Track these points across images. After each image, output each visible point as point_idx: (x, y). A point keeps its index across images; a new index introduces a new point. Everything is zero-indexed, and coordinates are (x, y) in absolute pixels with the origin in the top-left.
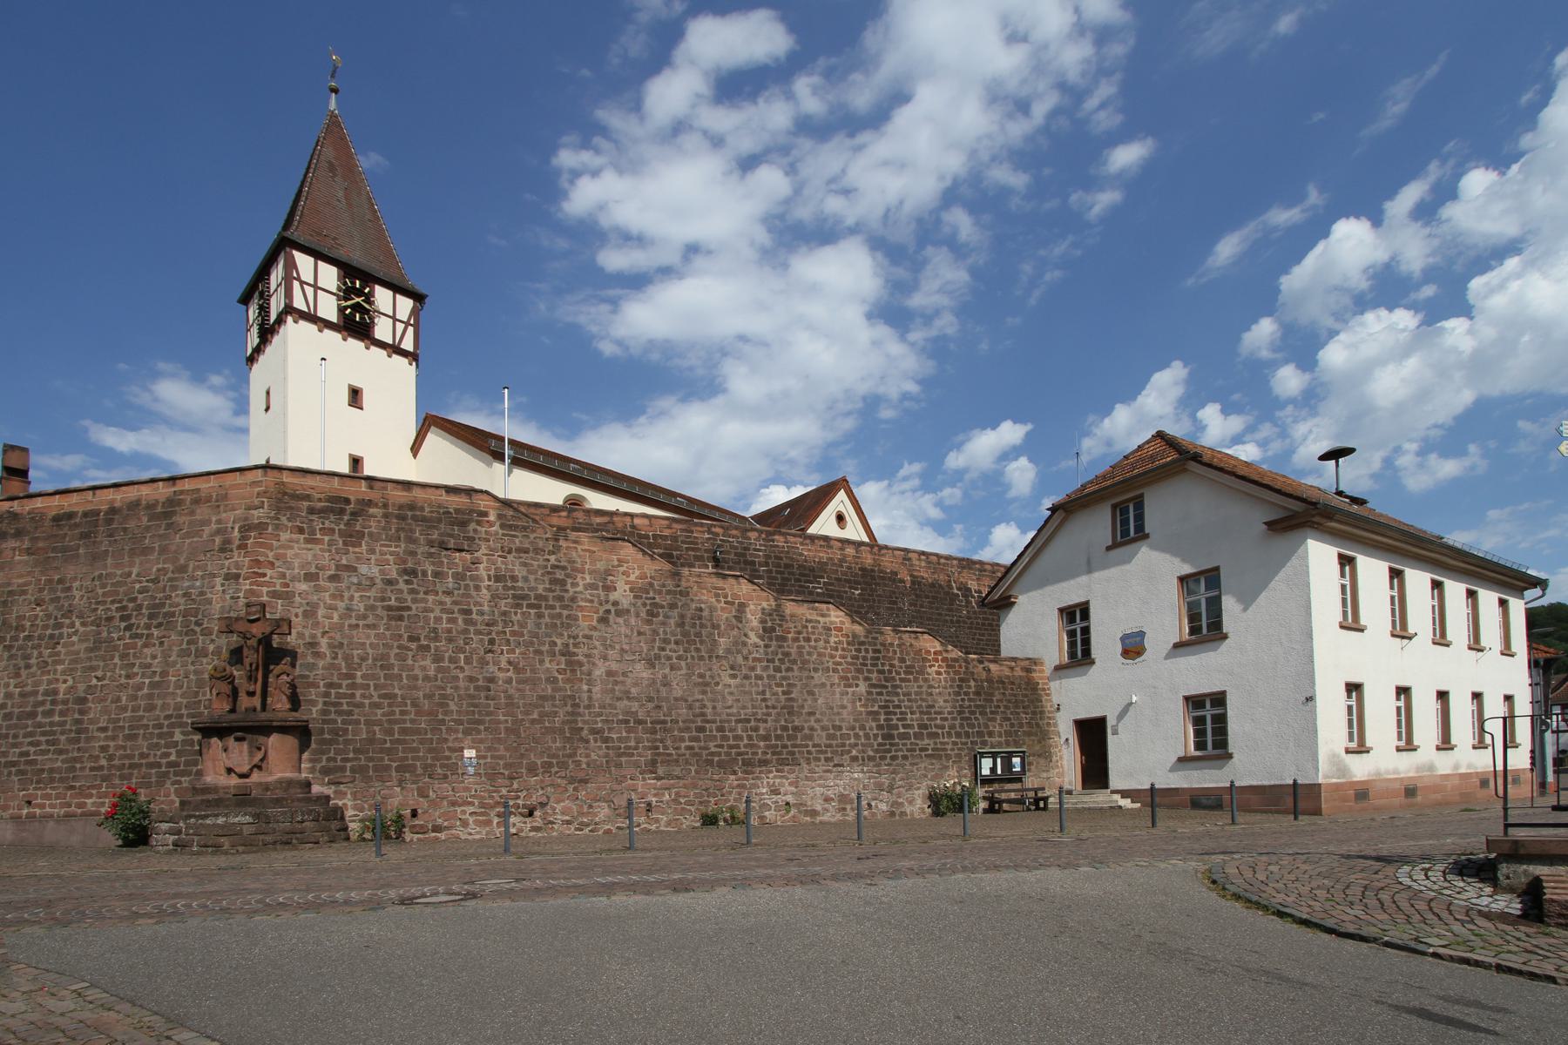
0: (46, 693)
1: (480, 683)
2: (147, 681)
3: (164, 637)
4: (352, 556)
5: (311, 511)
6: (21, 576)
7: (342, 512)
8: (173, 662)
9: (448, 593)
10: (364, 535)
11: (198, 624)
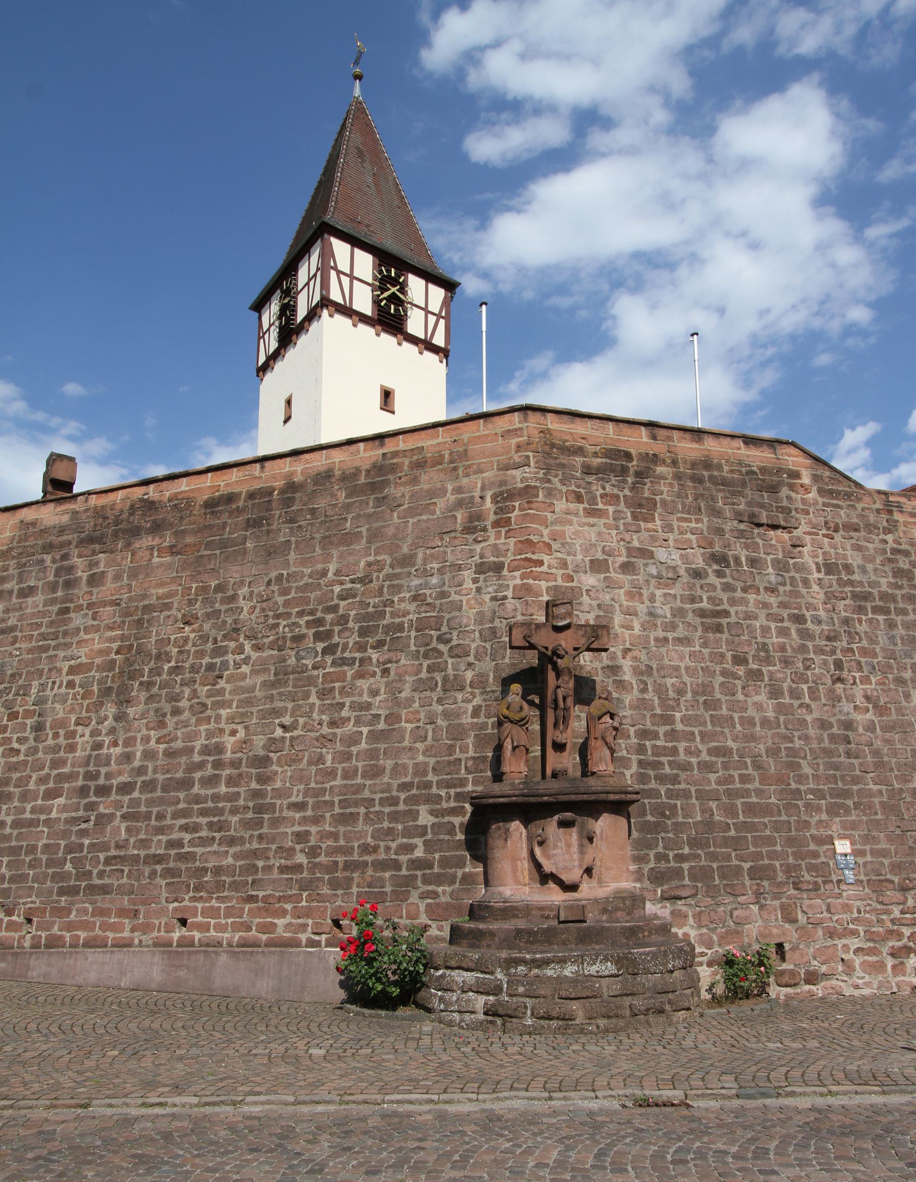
0: (206, 751)
1: (835, 730)
2: (365, 730)
3: (390, 662)
4: (645, 535)
5: (588, 470)
6: (162, 584)
7: (624, 471)
8: (407, 699)
9: (772, 590)
10: (655, 505)
11: (441, 639)
